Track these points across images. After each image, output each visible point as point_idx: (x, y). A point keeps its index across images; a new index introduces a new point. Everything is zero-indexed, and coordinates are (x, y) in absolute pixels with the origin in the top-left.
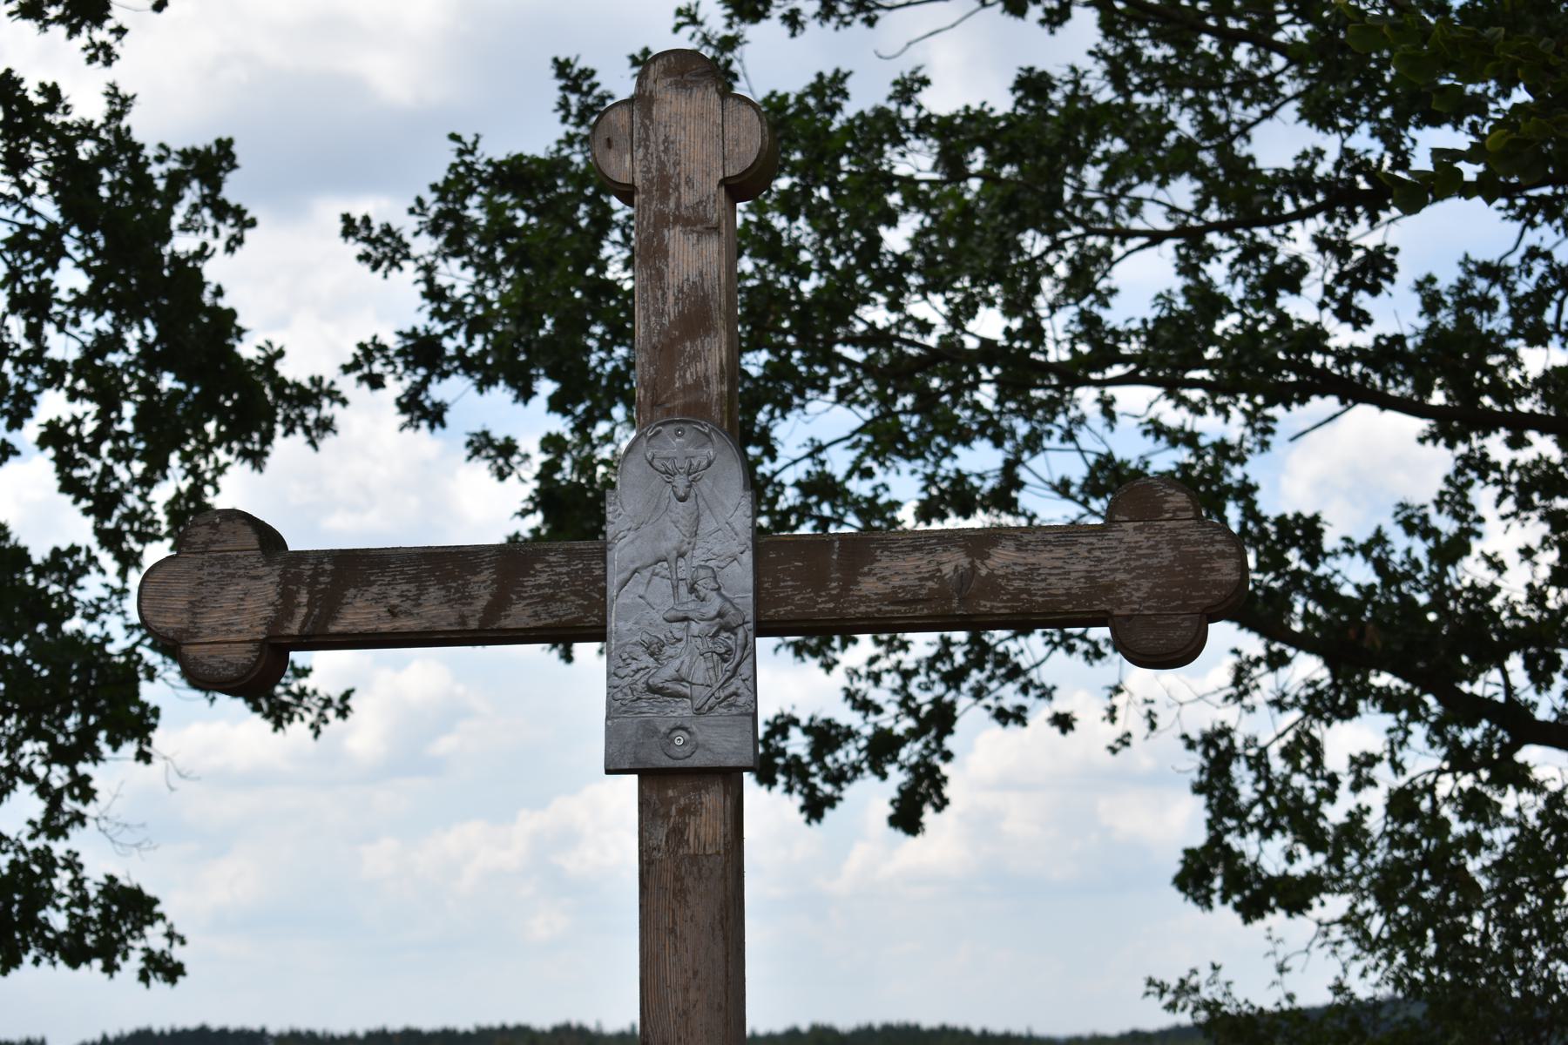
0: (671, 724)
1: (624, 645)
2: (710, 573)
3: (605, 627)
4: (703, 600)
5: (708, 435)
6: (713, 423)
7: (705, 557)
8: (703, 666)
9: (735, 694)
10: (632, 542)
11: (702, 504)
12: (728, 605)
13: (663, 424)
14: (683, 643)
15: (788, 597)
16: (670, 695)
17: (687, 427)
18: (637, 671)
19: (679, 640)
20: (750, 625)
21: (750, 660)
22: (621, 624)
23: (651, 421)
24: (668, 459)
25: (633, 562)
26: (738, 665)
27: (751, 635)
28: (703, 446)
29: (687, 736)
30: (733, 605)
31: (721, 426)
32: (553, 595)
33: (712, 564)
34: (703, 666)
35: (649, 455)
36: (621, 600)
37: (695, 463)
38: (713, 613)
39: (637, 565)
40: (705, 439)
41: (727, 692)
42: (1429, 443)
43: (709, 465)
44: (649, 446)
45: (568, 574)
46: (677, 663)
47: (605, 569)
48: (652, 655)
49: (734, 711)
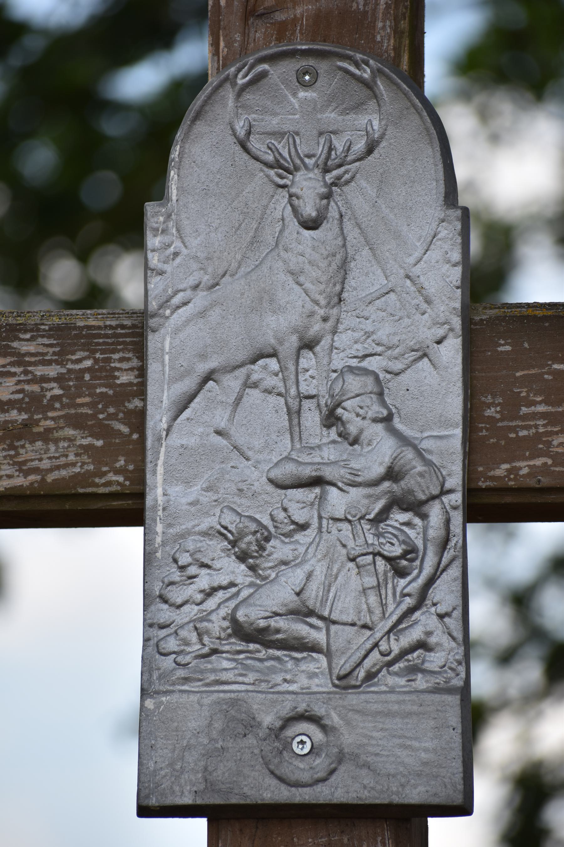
0: (286, 709)
1: (183, 536)
2: (370, 381)
3: (141, 496)
4: (355, 442)
5: (369, 85)
6: (378, 57)
7: (360, 349)
8: (355, 583)
9: (422, 645)
10: (202, 314)
11: (352, 234)
12: (409, 454)
13: (271, 59)
14: (311, 532)
15: (538, 437)
16: (284, 645)
17: (323, 66)
18: (214, 590)
19: (303, 527)
20: (457, 498)
21: (454, 571)
22: (176, 490)
23: (244, 51)
24: (280, 135)
25: (203, 357)
26: (431, 581)
27: (457, 518)
28: (357, 107)
29: (318, 735)
30: (419, 453)
31: (395, 64)
32: (26, 425)
33: (373, 364)
34: (355, 583)
35: (240, 128)
36: (175, 440)
37: (339, 144)
38: (378, 470)
39: (212, 364)
40: (362, 92)
41: (406, 640)
42: (170, 243)
43: (370, 150)
44: (240, 106)
45: (59, 379)
46: (299, 575)
47: (142, 372)
48: (243, 557)
49: (421, 682)
